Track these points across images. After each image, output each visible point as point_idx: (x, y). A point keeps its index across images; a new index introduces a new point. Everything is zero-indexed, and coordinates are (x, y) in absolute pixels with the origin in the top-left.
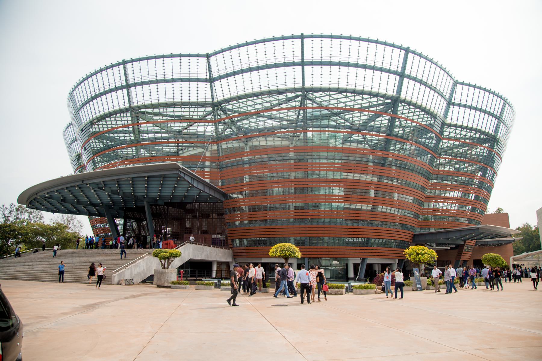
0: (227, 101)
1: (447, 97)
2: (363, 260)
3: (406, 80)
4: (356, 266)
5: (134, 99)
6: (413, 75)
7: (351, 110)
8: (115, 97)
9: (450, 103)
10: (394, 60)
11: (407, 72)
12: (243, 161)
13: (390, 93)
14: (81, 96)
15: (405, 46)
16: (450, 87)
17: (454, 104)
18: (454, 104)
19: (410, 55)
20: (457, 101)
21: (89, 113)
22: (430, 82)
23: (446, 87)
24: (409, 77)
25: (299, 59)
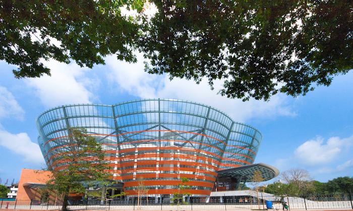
0: (121, 127)
1: (229, 128)
2: (189, 195)
3: (209, 121)
4: (186, 198)
5: (210, 114)
6: (213, 118)
7: (184, 133)
8: (53, 125)
9: (230, 131)
10: (204, 112)
11: (209, 117)
12: (245, 40)
13: (201, 125)
14: (43, 121)
15: (209, 106)
16: (231, 124)
17: (232, 131)
18: (232, 131)
19: (211, 110)
20: (234, 130)
21: (48, 129)
22: (225, 124)
23: (229, 125)
24: (210, 119)
25: (157, 109)
